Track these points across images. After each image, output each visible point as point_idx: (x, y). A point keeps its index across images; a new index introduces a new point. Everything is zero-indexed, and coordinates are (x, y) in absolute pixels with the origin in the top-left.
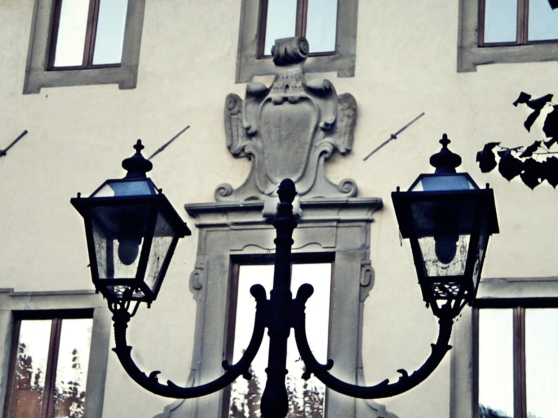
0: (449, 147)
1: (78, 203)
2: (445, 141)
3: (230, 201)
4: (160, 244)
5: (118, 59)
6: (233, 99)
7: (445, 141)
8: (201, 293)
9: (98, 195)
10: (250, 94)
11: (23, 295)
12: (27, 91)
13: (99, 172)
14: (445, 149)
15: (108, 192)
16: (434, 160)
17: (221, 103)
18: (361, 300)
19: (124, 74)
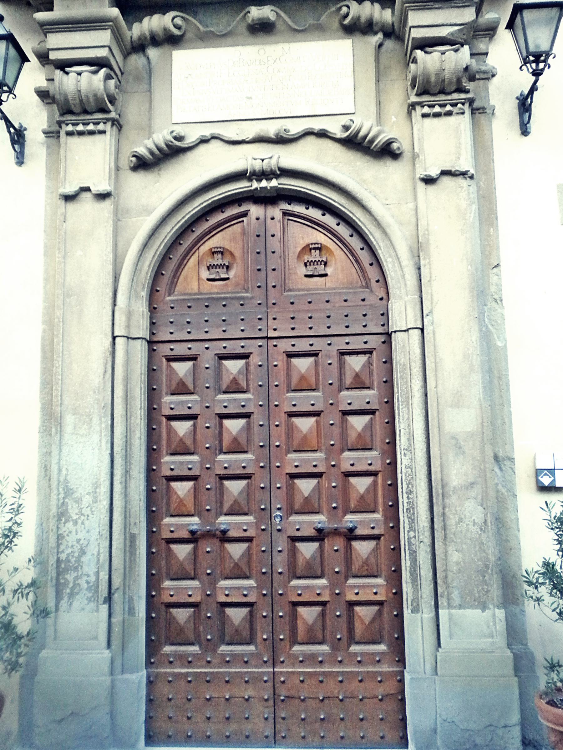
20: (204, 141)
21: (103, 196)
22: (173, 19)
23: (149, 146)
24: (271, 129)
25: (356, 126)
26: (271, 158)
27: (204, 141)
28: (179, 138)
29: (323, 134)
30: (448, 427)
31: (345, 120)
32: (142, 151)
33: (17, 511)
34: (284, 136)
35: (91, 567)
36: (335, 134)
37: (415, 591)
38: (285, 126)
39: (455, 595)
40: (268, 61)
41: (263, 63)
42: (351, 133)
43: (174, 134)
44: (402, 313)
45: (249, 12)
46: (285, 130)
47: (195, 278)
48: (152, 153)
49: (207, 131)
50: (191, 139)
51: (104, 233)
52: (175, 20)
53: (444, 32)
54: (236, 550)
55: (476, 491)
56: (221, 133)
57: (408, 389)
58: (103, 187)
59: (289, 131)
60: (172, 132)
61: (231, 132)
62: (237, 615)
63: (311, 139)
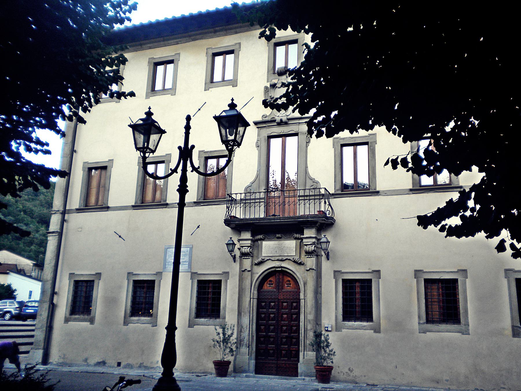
0: (234, 101)
1: (216, 118)
2: (233, 100)
3: (267, 119)
4: (241, 129)
5: (171, 87)
6: (266, 88)
7: (233, 100)
8: (259, 148)
9: (137, 123)
10: (271, 85)
11: (207, 152)
12: (205, 90)
13: (221, 108)
14: (232, 102)
15: (224, 114)
16: (229, 105)
17: (262, 89)
18: (307, 147)
19: (173, 91)
21: (249, 271)
24: (280, 258)
27: (268, 260)
29: (289, 260)
30: (308, 318)
31: (293, 257)
32: (256, 262)
33: (233, 330)
35: (246, 341)
37: (301, 348)
39: (308, 349)
44: (302, 296)
47: (267, 287)
51: (249, 278)
53: (309, 243)
54: (272, 339)
55: (312, 330)
57: (302, 310)
58: (249, 269)
62: (271, 351)
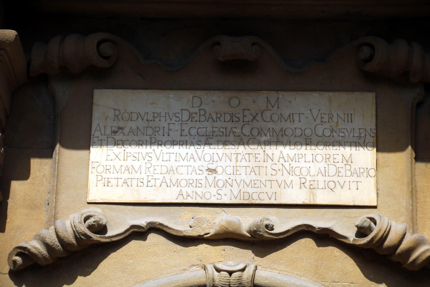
20: (138, 233)
22: (100, 43)
23: (48, 241)
24: (245, 221)
25: (380, 230)
26: (243, 270)
27: (138, 233)
28: (101, 229)
29: (325, 237)
34: (266, 235)
36: (345, 238)
38: (268, 219)
40: (244, 116)
41: (235, 119)
42: (372, 239)
43: (91, 221)
45: (218, 44)
46: (267, 226)
48: (47, 246)
49: (142, 219)
50: (113, 231)
52: (102, 46)
56: (166, 223)
59: (273, 229)
60: (87, 218)
61: (181, 222)
63: (307, 243)
